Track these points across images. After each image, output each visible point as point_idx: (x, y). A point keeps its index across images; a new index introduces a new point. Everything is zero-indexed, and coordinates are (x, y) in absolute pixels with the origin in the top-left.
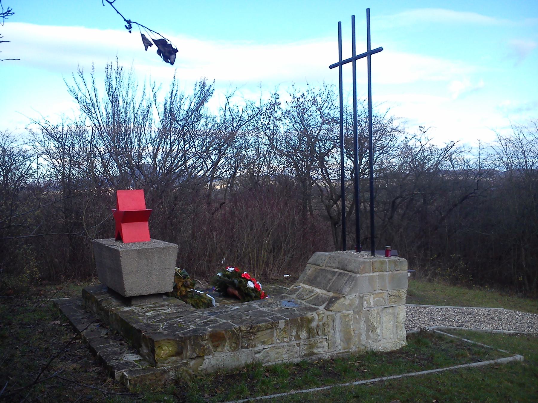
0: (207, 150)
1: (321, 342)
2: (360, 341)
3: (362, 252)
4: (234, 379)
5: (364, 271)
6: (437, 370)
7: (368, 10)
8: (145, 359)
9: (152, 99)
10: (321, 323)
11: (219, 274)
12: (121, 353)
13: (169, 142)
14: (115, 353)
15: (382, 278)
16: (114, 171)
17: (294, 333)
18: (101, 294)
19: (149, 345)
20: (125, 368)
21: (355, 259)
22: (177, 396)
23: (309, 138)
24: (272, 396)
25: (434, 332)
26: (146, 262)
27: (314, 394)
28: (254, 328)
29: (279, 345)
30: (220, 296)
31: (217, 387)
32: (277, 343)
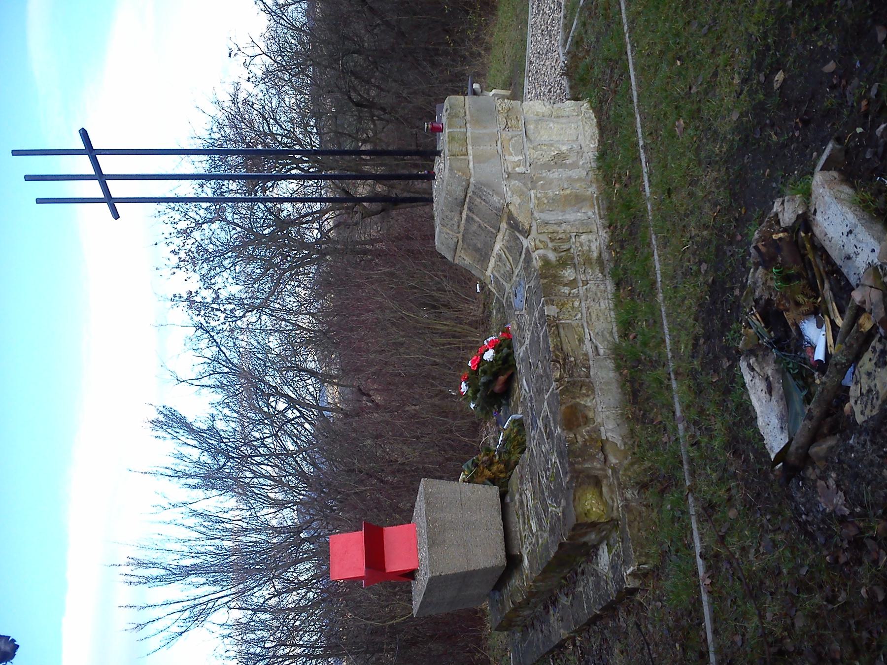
0: (268, 416)
1: (581, 245)
2: (580, 179)
3: (436, 170)
4: (639, 391)
5: (465, 171)
6: (629, 53)
7: (15, 153)
8: (606, 538)
9: (183, 509)
10: (550, 245)
11: (472, 406)
12: (596, 574)
13: (255, 480)
14: (597, 585)
15: (477, 140)
16: (304, 571)
17: (566, 290)
18: (502, 602)
19: (583, 531)
20: (621, 571)
21: (445, 183)
22: (666, 488)
23: (247, 245)
24: (666, 331)
25: (568, 53)
26: (450, 532)
27: (664, 264)
28: (557, 356)
29: (585, 315)
30: (508, 404)
31: (652, 421)
32: (581, 319)
